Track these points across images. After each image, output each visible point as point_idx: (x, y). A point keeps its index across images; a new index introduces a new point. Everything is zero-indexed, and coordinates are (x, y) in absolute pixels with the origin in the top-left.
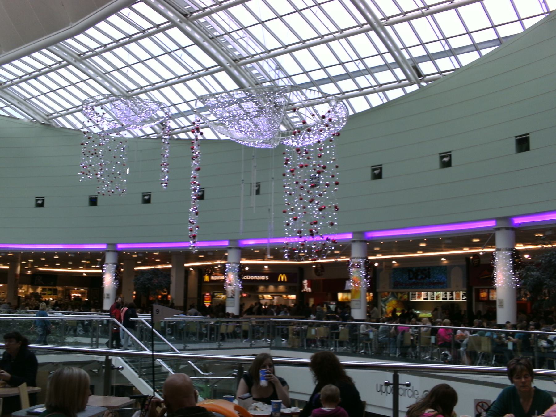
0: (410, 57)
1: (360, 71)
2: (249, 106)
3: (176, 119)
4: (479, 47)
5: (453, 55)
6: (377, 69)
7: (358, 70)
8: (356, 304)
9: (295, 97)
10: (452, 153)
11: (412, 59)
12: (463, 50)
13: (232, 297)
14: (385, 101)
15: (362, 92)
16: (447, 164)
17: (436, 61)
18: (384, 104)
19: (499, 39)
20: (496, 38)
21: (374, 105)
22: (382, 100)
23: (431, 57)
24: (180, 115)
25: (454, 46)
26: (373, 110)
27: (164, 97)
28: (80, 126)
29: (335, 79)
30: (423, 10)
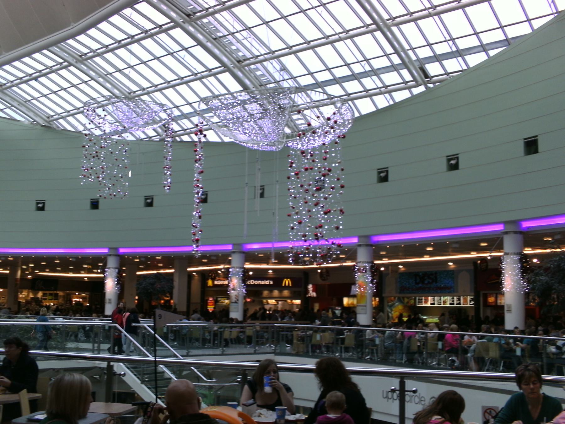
0: (417, 58)
1: (366, 72)
2: (254, 107)
3: (179, 121)
4: (487, 47)
5: (460, 56)
6: (383, 70)
7: (364, 71)
8: (362, 309)
9: (300, 99)
10: (459, 156)
11: (418, 60)
12: (470, 51)
13: (236, 302)
14: (391, 102)
15: (368, 94)
16: (454, 167)
17: (443, 62)
18: (390, 105)
19: (507, 40)
20: (504, 38)
21: (380, 107)
22: (388, 102)
23: (438, 58)
24: (183, 117)
25: (461, 47)
26: (379, 112)
27: (167, 99)
28: (81, 128)
29: (340, 80)
30: (430, 10)
